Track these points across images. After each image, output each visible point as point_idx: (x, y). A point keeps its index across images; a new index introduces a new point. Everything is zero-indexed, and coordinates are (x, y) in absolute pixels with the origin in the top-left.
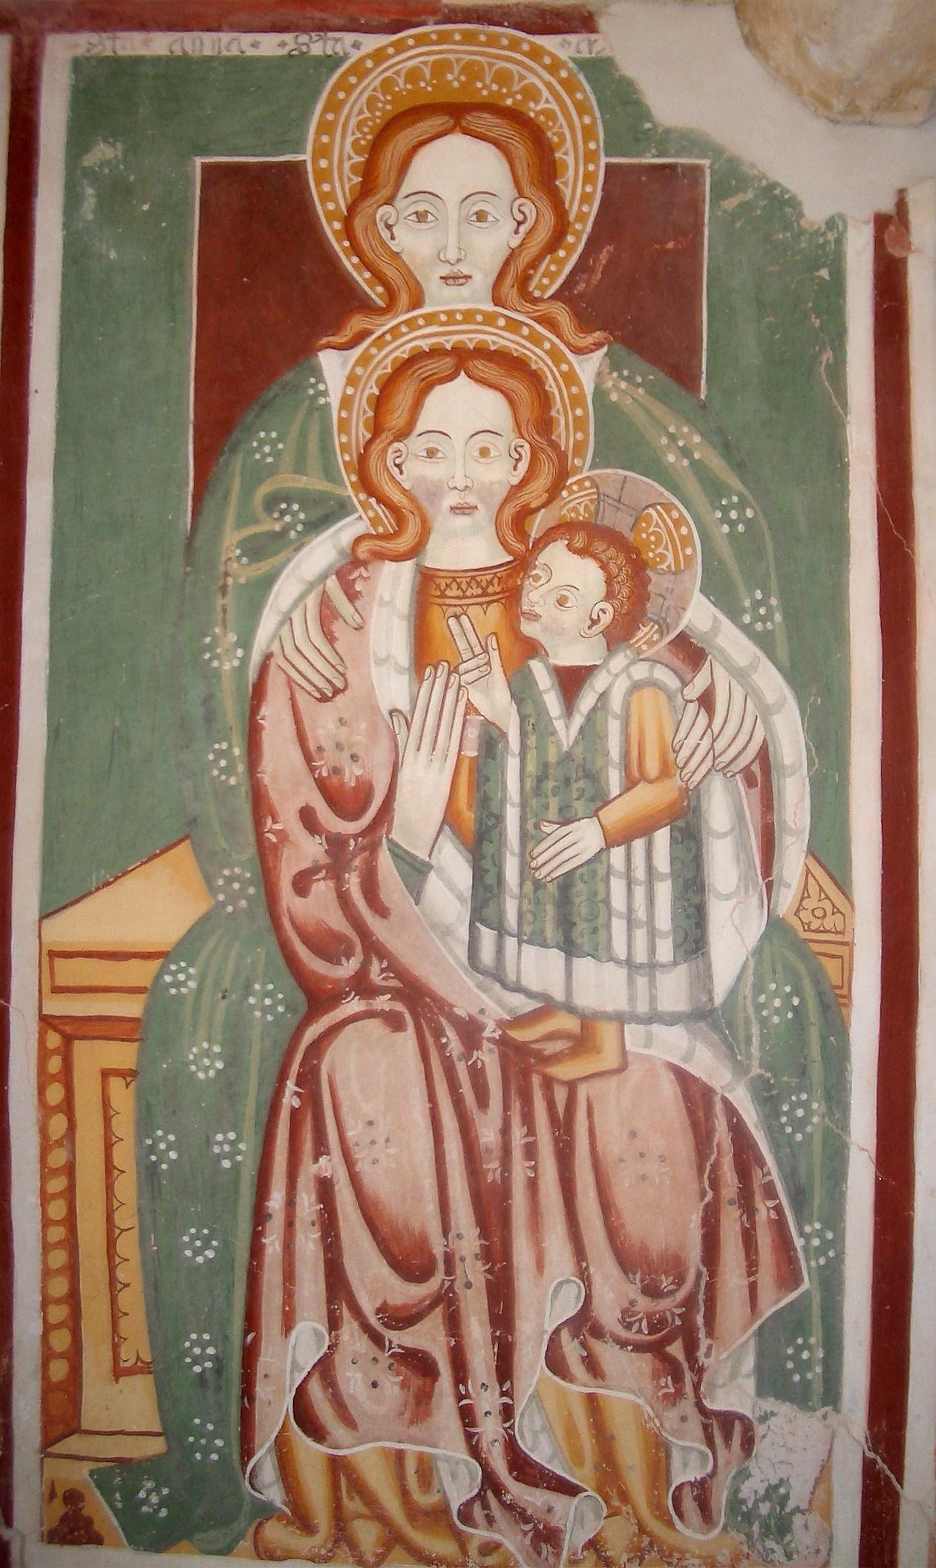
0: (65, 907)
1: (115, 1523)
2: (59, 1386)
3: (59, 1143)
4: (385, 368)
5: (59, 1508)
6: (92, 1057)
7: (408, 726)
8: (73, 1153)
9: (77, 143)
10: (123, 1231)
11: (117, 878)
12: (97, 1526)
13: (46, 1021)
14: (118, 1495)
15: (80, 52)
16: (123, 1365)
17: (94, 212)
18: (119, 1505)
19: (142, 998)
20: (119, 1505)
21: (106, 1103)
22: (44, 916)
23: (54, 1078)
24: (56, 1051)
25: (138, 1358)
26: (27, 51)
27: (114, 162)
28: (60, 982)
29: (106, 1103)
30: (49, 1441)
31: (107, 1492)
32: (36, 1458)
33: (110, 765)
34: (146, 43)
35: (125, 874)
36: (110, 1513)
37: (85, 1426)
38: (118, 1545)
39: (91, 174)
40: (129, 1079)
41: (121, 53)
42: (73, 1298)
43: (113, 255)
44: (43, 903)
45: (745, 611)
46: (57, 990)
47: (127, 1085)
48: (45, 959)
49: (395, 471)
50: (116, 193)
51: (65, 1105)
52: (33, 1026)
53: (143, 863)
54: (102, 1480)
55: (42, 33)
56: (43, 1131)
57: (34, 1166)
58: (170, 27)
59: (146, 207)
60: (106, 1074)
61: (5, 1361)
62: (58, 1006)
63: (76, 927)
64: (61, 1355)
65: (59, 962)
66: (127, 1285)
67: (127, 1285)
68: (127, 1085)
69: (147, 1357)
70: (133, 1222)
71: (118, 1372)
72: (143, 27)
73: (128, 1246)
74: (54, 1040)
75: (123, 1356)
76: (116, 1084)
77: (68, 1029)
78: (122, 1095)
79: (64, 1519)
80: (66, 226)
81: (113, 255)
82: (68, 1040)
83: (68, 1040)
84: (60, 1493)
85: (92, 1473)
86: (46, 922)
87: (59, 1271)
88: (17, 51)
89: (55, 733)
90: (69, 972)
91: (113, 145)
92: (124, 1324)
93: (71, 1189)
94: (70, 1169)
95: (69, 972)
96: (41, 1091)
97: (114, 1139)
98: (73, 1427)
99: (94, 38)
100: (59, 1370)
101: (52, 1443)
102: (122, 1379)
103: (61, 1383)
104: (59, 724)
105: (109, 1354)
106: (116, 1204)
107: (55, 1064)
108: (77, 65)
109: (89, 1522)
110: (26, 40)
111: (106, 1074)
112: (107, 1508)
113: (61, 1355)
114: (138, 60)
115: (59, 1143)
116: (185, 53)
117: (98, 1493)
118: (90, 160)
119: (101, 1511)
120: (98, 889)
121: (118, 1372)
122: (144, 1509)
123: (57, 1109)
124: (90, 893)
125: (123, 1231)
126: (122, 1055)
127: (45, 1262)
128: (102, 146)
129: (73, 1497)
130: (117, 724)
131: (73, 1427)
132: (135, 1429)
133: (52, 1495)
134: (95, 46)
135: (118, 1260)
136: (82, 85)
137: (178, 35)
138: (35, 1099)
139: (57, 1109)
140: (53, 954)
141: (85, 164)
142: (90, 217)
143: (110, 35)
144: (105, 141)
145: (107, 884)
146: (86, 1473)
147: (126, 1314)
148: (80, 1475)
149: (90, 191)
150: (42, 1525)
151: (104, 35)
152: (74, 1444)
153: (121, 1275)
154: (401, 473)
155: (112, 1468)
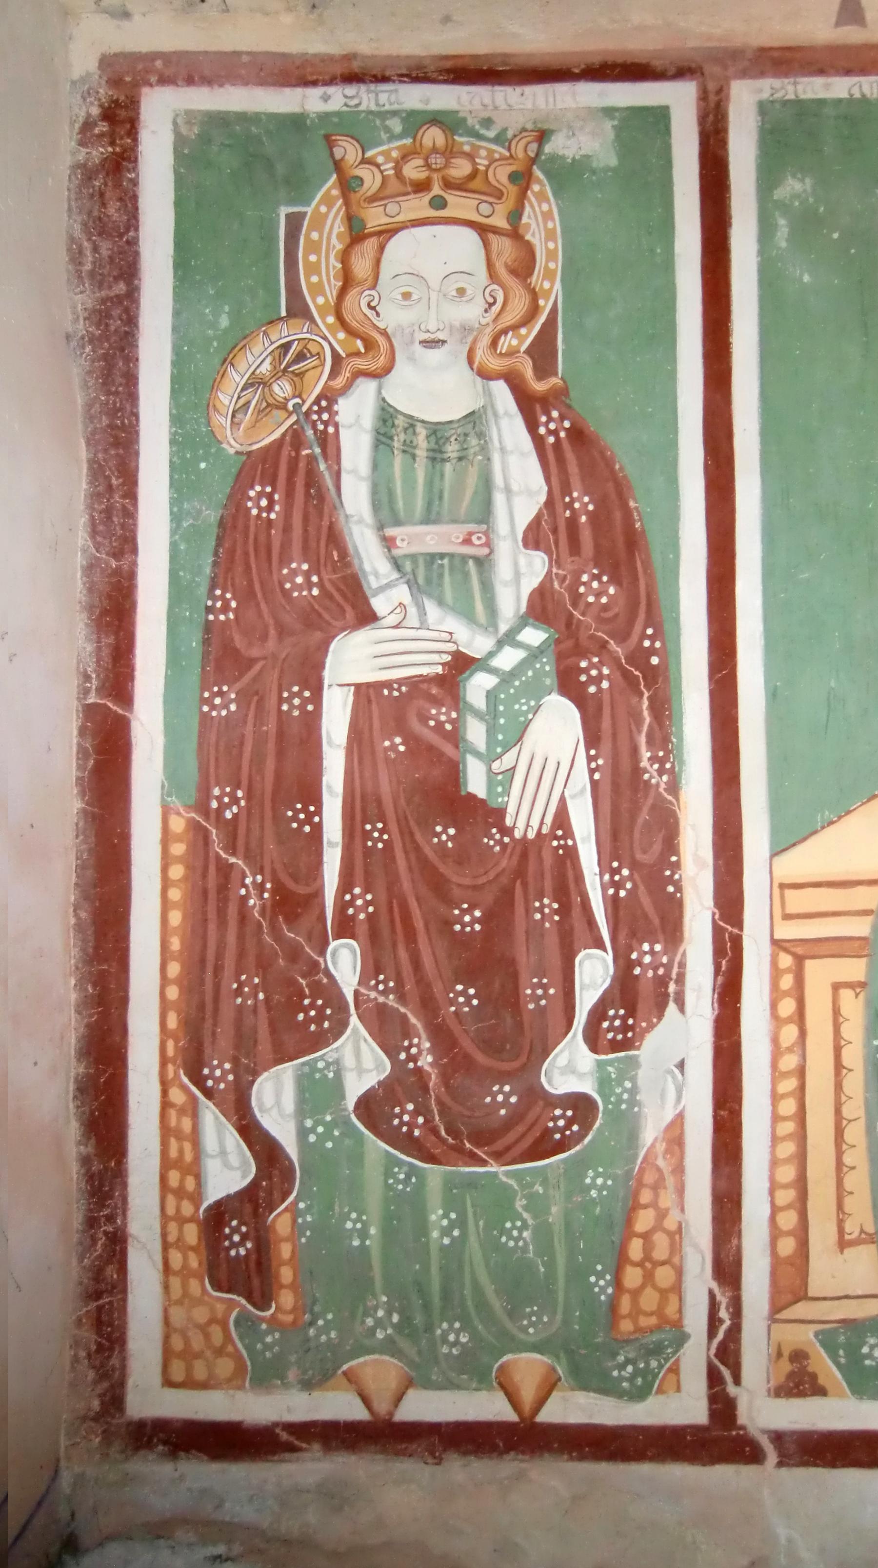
0: (794, 845)
1: (839, 1375)
2: (789, 1261)
3: (790, 1050)
4: (533, 235)
5: (786, 1367)
6: (820, 974)
7: (396, 627)
8: (804, 1057)
9: (768, 178)
10: (850, 1121)
11: (840, 818)
12: (821, 1381)
13: (777, 944)
14: (841, 1352)
15: (765, 95)
16: (847, 1237)
17: (787, 240)
18: (843, 1361)
19: (869, 919)
20: (843, 1361)
21: (836, 1012)
22: (774, 854)
23: (786, 994)
24: (787, 970)
25: (862, 1231)
26: (713, 98)
27: (804, 195)
28: (791, 909)
29: (836, 1012)
30: (776, 1308)
31: (831, 1348)
32: (763, 1324)
33: (828, 721)
34: (827, 86)
35: (848, 812)
36: (834, 1369)
37: (811, 1294)
38: (841, 1395)
39: (784, 207)
40: (858, 990)
41: (802, 96)
42: (801, 1184)
43: (806, 278)
44: (774, 841)
45: (566, 430)
46: (787, 917)
47: (857, 995)
48: (776, 891)
49: (370, 313)
50: (807, 224)
51: (796, 1018)
52: (766, 949)
53: (863, 804)
54: (827, 1340)
55: (727, 80)
56: (775, 1041)
57: (767, 1072)
58: (848, 72)
59: (836, 236)
60: (836, 987)
61: (735, 1242)
62: (788, 931)
63: (792, 865)
64: (789, 1233)
65: (788, 893)
66: (853, 1168)
67: (853, 1168)
68: (857, 995)
69: (870, 1228)
70: (861, 1113)
71: (843, 1244)
72: (821, 72)
73: (855, 1133)
74: (786, 961)
75: (848, 1227)
76: (846, 995)
77: (799, 950)
78: (853, 1007)
79: (791, 1375)
80: (761, 253)
81: (806, 278)
82: (800, 960)
83: (800, 960)
84: (786, 1354)
85: (816, 1334)
86: (776, 860)
87: (787, 1161)
88: (703, 96)
89: (773, 695)
90: (797, 901)
91: (802, 181)
92: (848, 1201)
93: (802, 1087)
94: (801, 1072)
95: (797, 901)
96: (774, 1006)
97: (843, 1043)
98: (801, 1295)
99: (777, 83)
100: (787, 1246)
101: (779, 1310)
102: (846, 1251)
103: (789, 1257)
104: (776, 686)
105: (834, 1229)
106: (844, 1098)
107: (787, 982)
108: (763, 108)
109: (814, 1377)
110: (712, 86)
111: (836, 987)
112: (829, 1362)
113: (789, 1233)
114: (822, 102)
115: (790, 1050)
116: (863, 95)
117: (822, 1351)
118: (779, 194)
119: (826, 1367)
120: (823, 828)
121: (843, 1244)
122: (868, 1362)
123: (789, 1020)
124: (815, 832)
125: (850, 1121)
126: (854, 969)
127: (773, 1153)
128: (790, 181)
129: (799, 1356)
130: (833, 684)
131: (801, 1295)
132: (860, 1293)
133: (779, 1355)
134: (777, 91)
135: (845, 1147)
136: (768, 126)
137: (855, 79)
138: (768, 1013)
139: (789, 1020)
140: (782, 886)
141: (775, 198)
142: (784, 244)
143: (792, 80)
144: (794, 176)
145: (831, 823)
146: (811, 1336)
147: (851, 1193)
148: (806, 1336)
149: (782, 222)
150: (768, 1382)
151: (786, 81)
152: (800, 1310)
153: (848, 1159)
154: (378, 314)
155: (836, 1329)
